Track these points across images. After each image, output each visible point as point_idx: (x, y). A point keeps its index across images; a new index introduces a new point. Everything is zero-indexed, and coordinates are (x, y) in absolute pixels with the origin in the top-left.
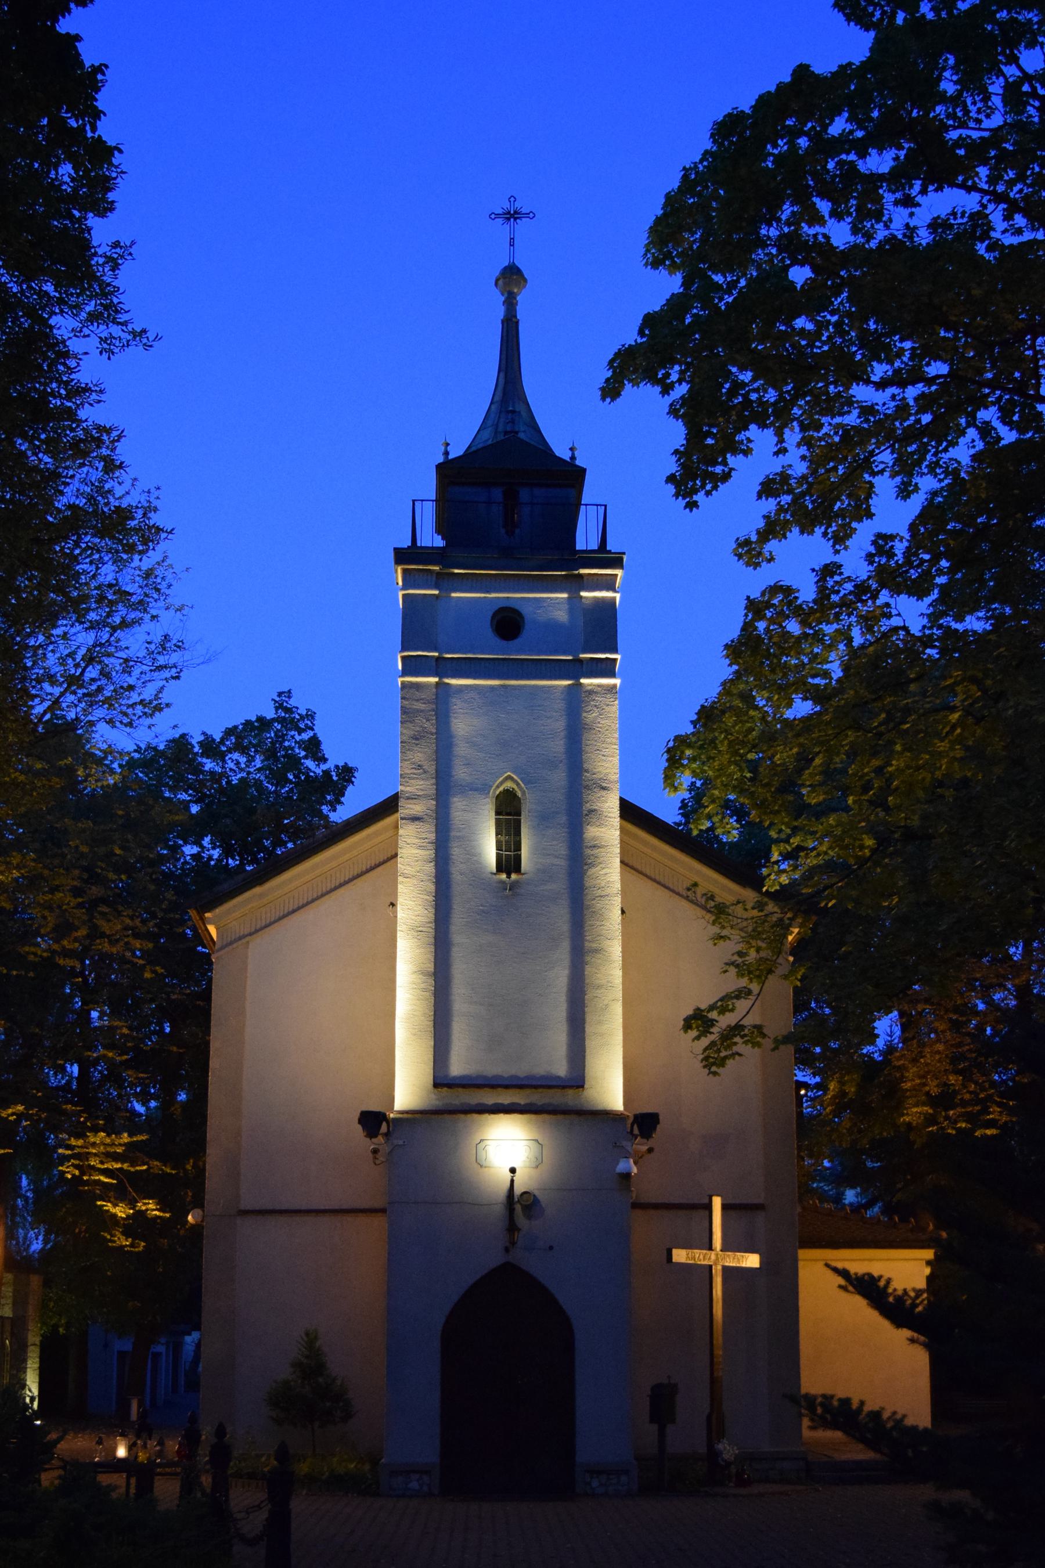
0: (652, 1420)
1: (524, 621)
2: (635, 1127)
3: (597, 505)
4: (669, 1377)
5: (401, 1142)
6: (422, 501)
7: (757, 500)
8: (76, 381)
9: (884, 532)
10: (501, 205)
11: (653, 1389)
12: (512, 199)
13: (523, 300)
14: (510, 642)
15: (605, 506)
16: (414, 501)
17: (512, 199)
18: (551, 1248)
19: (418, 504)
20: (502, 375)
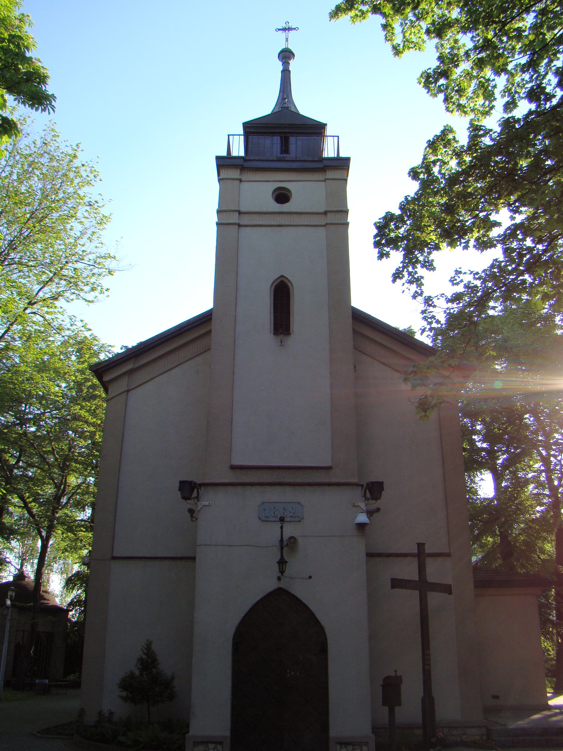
0: (384, 704)
1: (291, 194)
2: (367, 491)
3: (333, 136)
4: (396, 671)
5: (207, 503)
6: (233, 135)
7: (434, 269)
8: (15, 9)
9: (494, 490)
10: (282, 25)
11: (384, 680)
12: (287, 23)
13: (293, 65)
14: (284, 205)
15: (338, 137)
16: (229, 135)
17: (287, 23)
18: (310, 577)
19: (231, 137)
20: (281, 94)
